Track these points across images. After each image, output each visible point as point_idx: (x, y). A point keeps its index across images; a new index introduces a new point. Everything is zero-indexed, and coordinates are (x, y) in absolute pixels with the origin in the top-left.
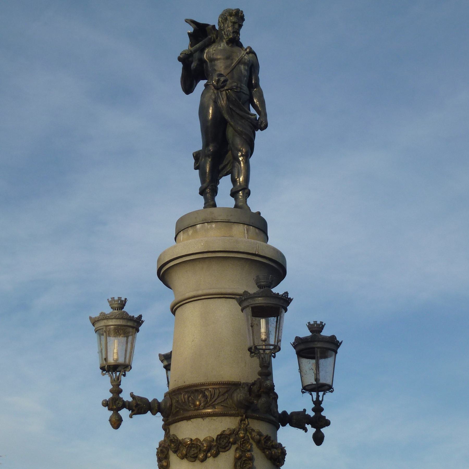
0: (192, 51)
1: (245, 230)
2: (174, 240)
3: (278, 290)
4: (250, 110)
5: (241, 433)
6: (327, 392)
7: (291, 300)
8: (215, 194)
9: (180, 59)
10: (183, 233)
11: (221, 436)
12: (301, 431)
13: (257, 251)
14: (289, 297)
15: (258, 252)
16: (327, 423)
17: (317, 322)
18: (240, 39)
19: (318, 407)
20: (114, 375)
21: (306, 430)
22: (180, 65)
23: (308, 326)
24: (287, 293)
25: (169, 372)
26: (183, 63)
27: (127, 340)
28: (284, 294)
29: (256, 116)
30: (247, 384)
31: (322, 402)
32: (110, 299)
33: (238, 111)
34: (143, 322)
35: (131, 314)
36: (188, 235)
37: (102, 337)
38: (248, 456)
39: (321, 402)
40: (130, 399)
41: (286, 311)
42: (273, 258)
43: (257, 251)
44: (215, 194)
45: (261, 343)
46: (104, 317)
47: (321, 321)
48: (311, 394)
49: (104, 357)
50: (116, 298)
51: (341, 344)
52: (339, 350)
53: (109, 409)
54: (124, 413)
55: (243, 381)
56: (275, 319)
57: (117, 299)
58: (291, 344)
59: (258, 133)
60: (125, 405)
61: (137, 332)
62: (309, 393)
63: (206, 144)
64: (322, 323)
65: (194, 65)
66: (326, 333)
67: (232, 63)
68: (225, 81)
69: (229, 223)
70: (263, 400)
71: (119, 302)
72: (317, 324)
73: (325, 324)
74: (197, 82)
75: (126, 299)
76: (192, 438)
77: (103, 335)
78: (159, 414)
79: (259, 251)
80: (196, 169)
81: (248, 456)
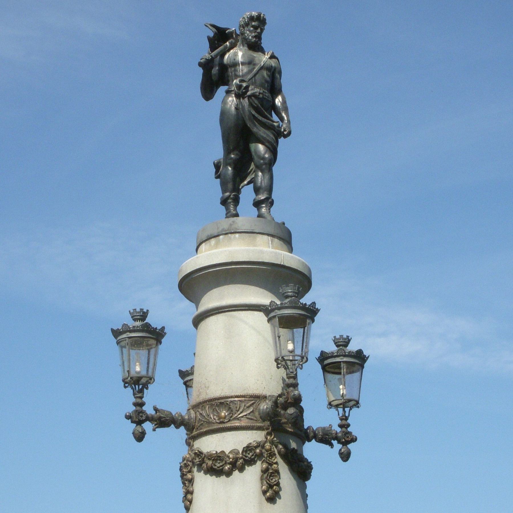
0: (213, 56)
1: (269, 240)
2: (195, 251)
3: (307, 300)
4: (272, 116)
5: (267, 445)
6: (353, 408)
7: (318, 310)
8: (237, 204)
9: (200, 64)
10: (205, 244)
11: (248, 448)
12: (327, 447)
13: (282, 261)
14: (316, 307)
15: (283, 262)
16: (354, 440)
17: (343, 336)
18: (262, 43)
19: (344, 425)
20: (137, 386)
21: (332, 445)
22: (201, 71)
23: (334, 341)
24: (314, 303)
25: (189, 389)
26: (203, 69)
27: (149, 352)
28: (311, 304)
29: (279, 123)
30: (273, 396)
31: (348, 417)
32: (132, 311)
33: (260, 118)
34: (165, 334)
35: (154, 325)
36: (210, 245)
37: (124, 349)
38: (275, 469)
39: (346, 419)
40: (153, 412)
41: (313, 321)
42: (299, 269)
43: (282, 261)
44: (237, 204)
45: (288, 354)
46: (126, 329)
47: (348, 335)
48: (337, 410)
49: (126, 369)
50: (138, 310)
51: (368, 359)
52: (366, 365)
53: (132, 422)
54: (148, 426)
55: (268, 394)
56: (301, 330)
57: (139, 310)
58: (316, 359)
59: (281, 140)
60: (149, 419)
61: (159, 344)
62: (335, 409)
63: (227, 151)
64: (348, 337)
65: (215, 70)
66: (352, 347)
67: (254, 68)
68: (247, 88)
69: (253, 235)
70: (291, 411)
71: (141, 313)
72: (343, 339)
73: (351, 338)
74: (218, 88)
75: (148, 311)
76: (218, 451)
77: (125, 347)
78: (182, 428)
79: (284, 262)
80: (216, 178)
81: (275, 469)
